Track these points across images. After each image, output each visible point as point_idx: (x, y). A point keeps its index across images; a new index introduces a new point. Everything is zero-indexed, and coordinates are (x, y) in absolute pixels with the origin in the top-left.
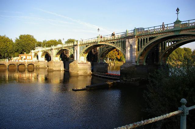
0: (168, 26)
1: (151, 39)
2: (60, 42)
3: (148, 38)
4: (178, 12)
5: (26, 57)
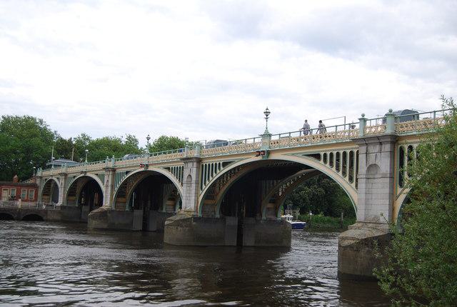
0: (437, 116)
1: (225, 164)
2: (129, 148)
3: (221, 163)
4: (267, 115)
5: (19, 192)
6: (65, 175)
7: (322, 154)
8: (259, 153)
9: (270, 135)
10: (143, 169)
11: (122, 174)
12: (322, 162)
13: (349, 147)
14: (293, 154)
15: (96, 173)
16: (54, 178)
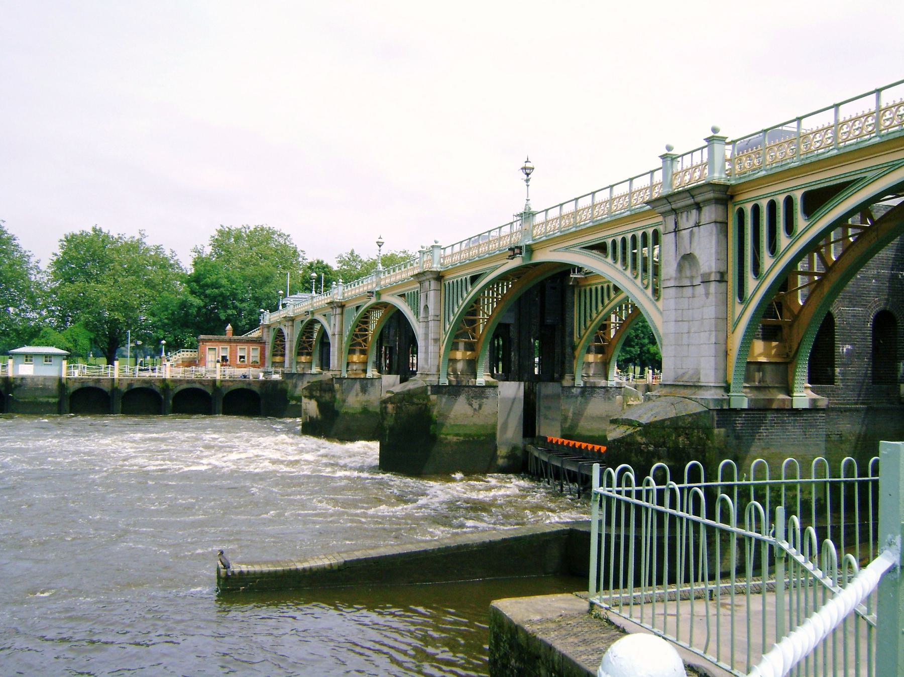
3: (798, 196)
4: (528, 175)
6: (292, 320)
7: (609, 242)
8: (514, 251)
9: (533, 214)
10: (517, 262)
11: (461, 286)
12: (610, 259)
13: (411, 287)
14: (567, 249)
15: (401, 291)
16: (318, 317)
